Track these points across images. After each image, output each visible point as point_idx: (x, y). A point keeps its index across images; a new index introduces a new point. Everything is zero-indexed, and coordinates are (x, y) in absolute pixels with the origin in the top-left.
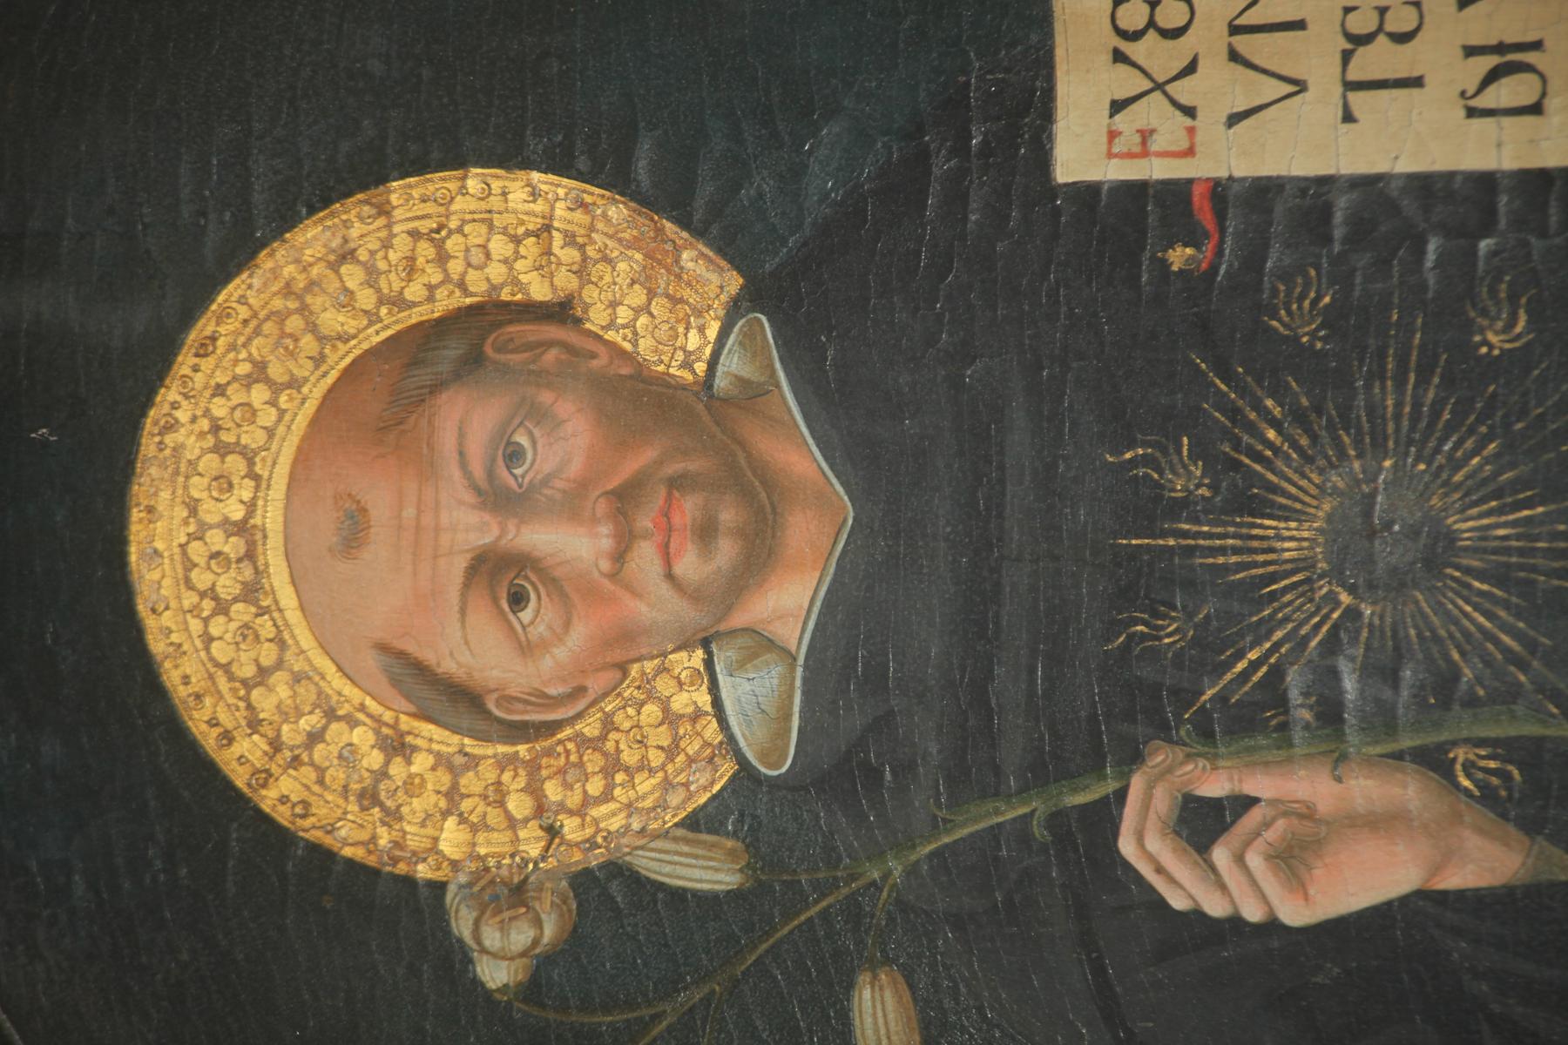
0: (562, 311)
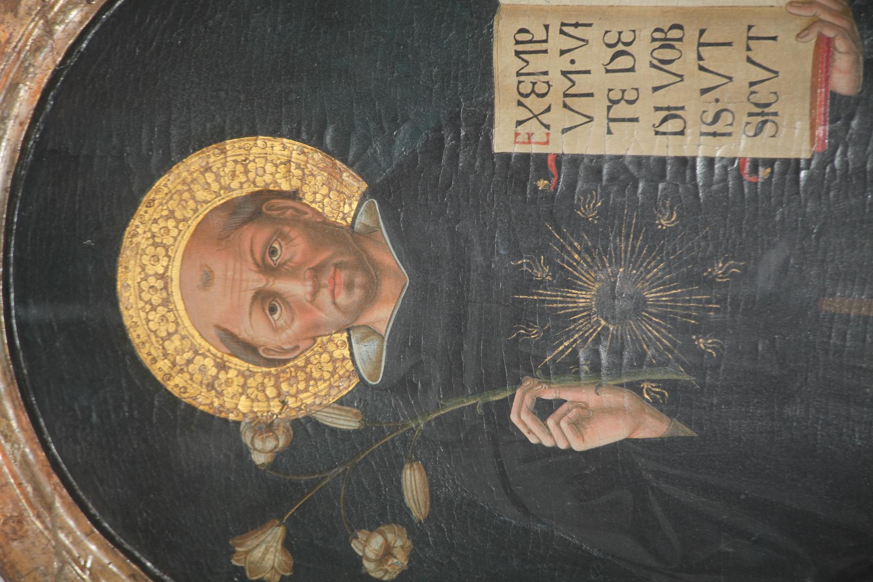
0: (294, 195)
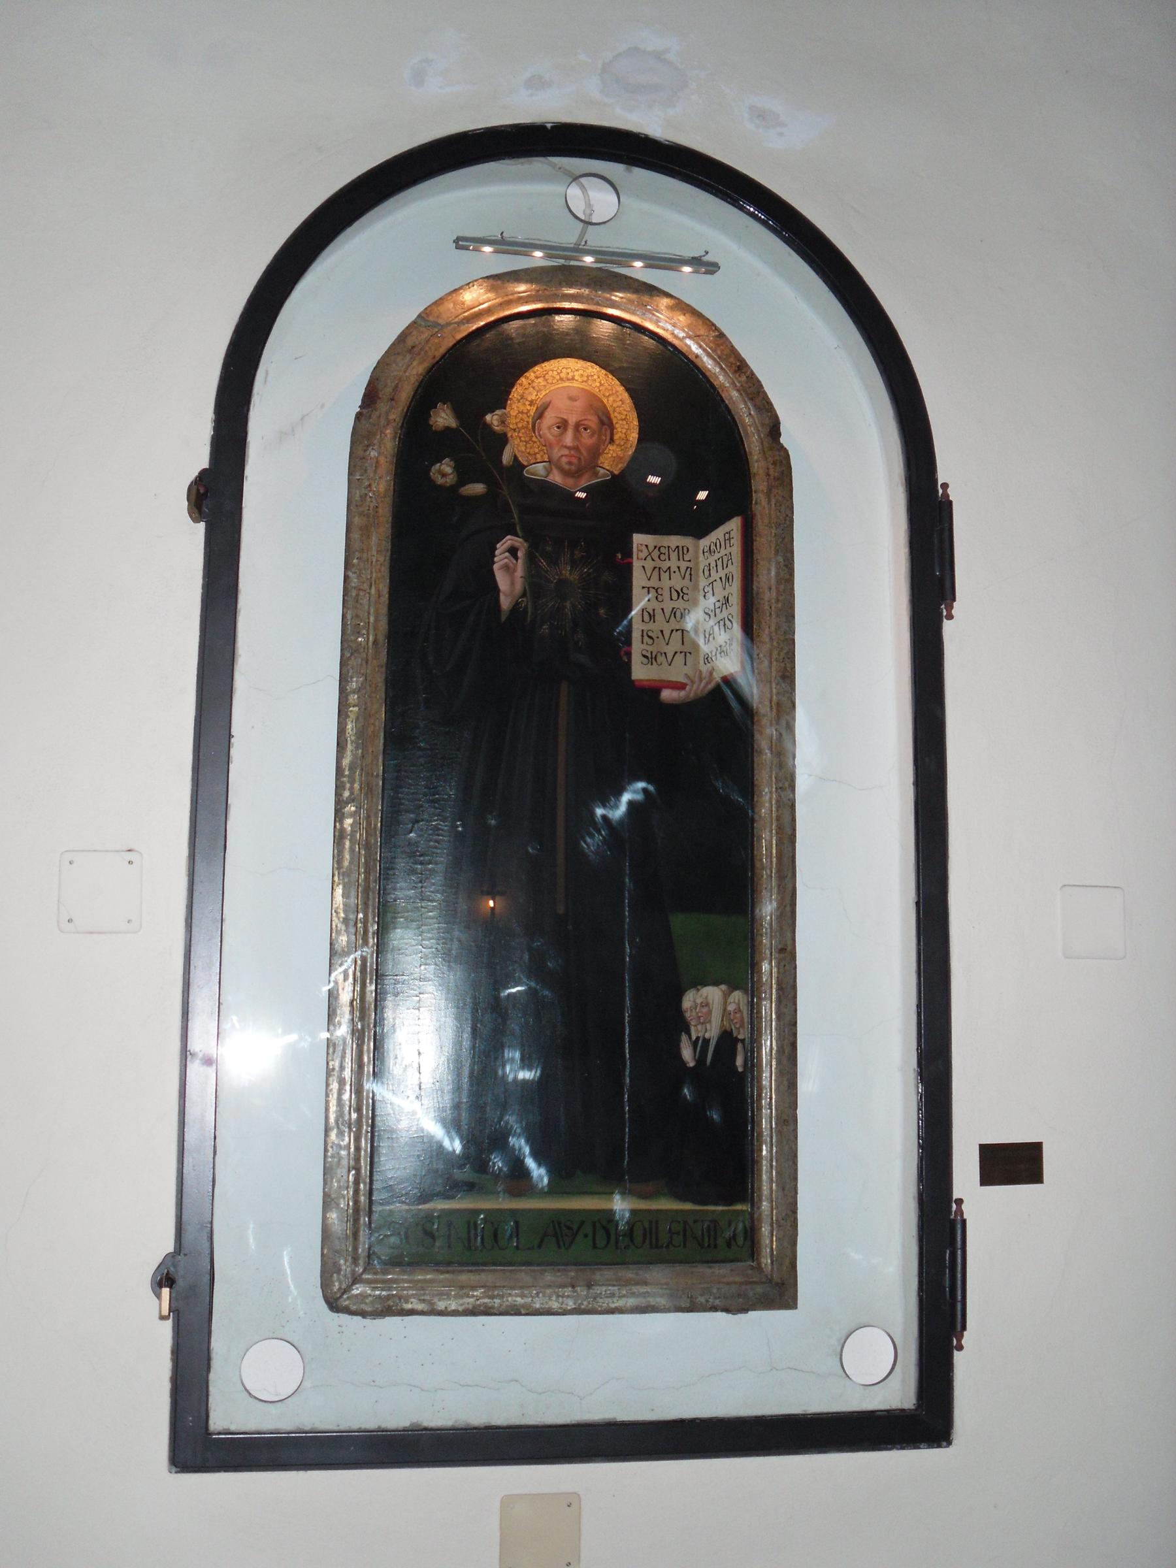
0: (612, 441)
